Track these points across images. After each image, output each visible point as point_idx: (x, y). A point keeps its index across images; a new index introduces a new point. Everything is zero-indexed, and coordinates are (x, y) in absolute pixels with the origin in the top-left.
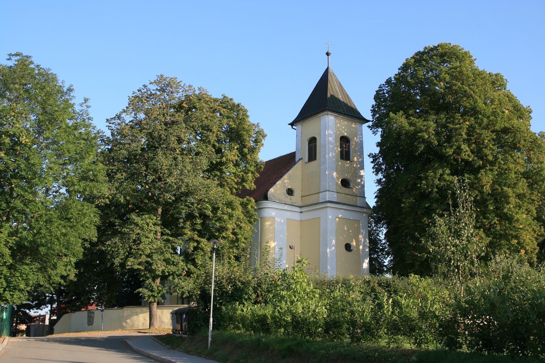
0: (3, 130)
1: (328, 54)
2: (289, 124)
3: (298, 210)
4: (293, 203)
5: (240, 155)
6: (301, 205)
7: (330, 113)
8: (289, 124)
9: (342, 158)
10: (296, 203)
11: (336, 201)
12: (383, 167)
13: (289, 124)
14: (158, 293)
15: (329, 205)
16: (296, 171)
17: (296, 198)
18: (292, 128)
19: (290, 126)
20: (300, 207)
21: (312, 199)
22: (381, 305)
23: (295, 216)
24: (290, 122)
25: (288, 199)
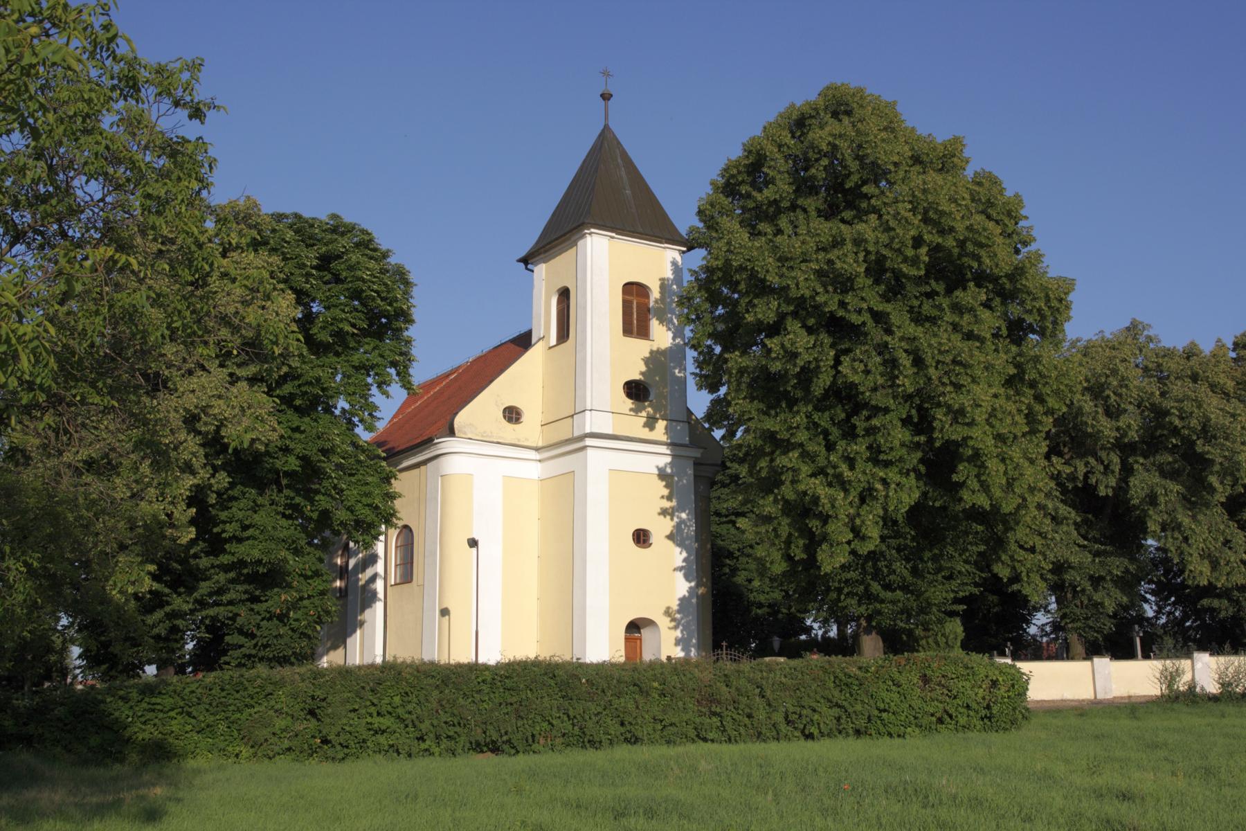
0: (4, 301)
1: (606, 97)
3: (533, 455)
4: (519, 440)
5: (1064, 510)
6: (540, 444)
7: (593, 230)
8: (520, 261)
10: (527, 439)
11: (610, 432)
12: (718, 434)
14: (144, 730)
15: (589, 442)
16: (532, 364)
17: (531, 429)
18: (527, 269)
19: (522, 265)
20: (537, 449)
21: (563, 432)
22: (727, 184)
23: (531, 469)
24: (523, 254)
25: (510, 431)
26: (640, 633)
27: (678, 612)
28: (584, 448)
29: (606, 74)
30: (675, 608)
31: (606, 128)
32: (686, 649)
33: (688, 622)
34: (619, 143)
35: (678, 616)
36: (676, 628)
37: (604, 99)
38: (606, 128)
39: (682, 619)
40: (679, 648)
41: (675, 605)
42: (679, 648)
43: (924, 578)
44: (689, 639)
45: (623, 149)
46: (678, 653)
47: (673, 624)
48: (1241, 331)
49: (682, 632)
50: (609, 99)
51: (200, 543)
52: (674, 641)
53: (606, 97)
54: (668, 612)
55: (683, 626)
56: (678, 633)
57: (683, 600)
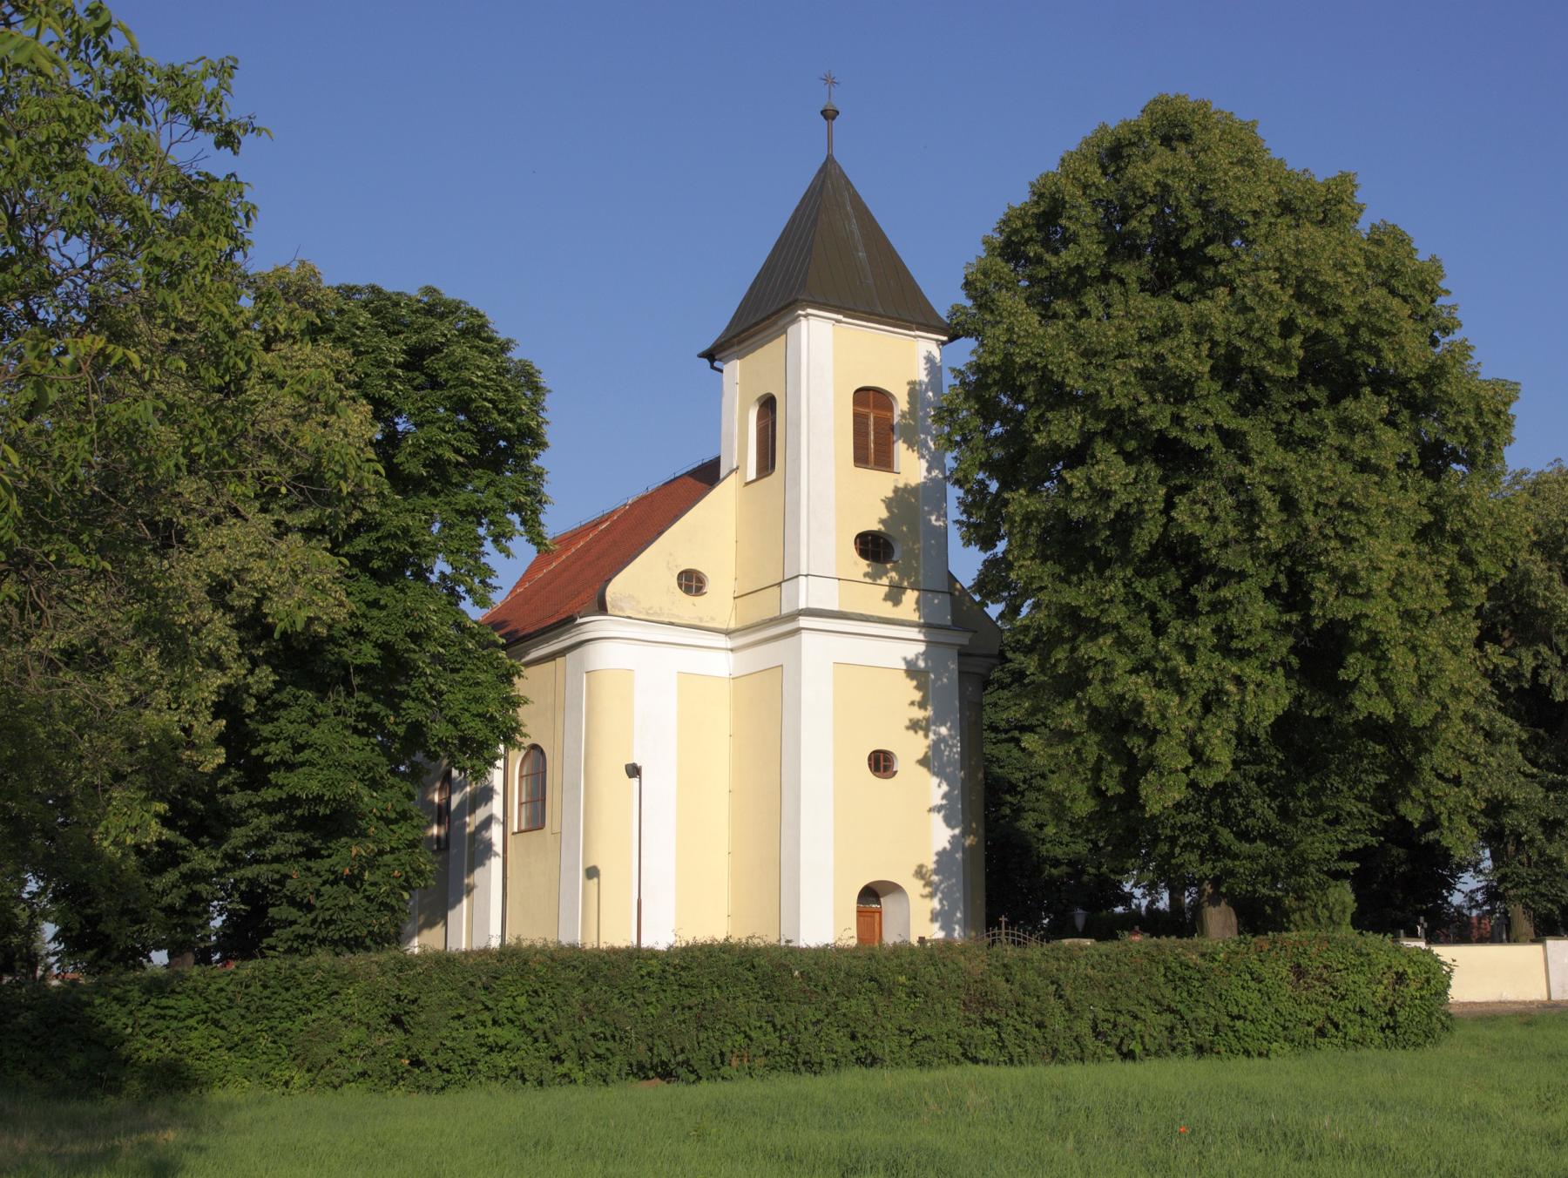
1: (829, 115)
2: (702, 356)
7: (810, 311)
9: (861, 459)
11: (835, 607)
13: (702, 356)
18: (713, 367)
19: (706, 362)
26: (879, 903)
27: (936, 872)
28: (798, 630)
29: (830, 81)
30: (931, 866)
31: (830, 160)
34: (848, 182)
35: (935, 878)
37: (826, 118)
38: (830, 160)
39: (941, 882)
40: (937, 925)
41: (930, 863)
42: (937, 925)
43: (1298, 822)
47: (928, 890)
49: (941, 901)
50: (833, 119)
53: (829, 115)
54: (920, 873)
55: (942, 892)
56: (935, 904)
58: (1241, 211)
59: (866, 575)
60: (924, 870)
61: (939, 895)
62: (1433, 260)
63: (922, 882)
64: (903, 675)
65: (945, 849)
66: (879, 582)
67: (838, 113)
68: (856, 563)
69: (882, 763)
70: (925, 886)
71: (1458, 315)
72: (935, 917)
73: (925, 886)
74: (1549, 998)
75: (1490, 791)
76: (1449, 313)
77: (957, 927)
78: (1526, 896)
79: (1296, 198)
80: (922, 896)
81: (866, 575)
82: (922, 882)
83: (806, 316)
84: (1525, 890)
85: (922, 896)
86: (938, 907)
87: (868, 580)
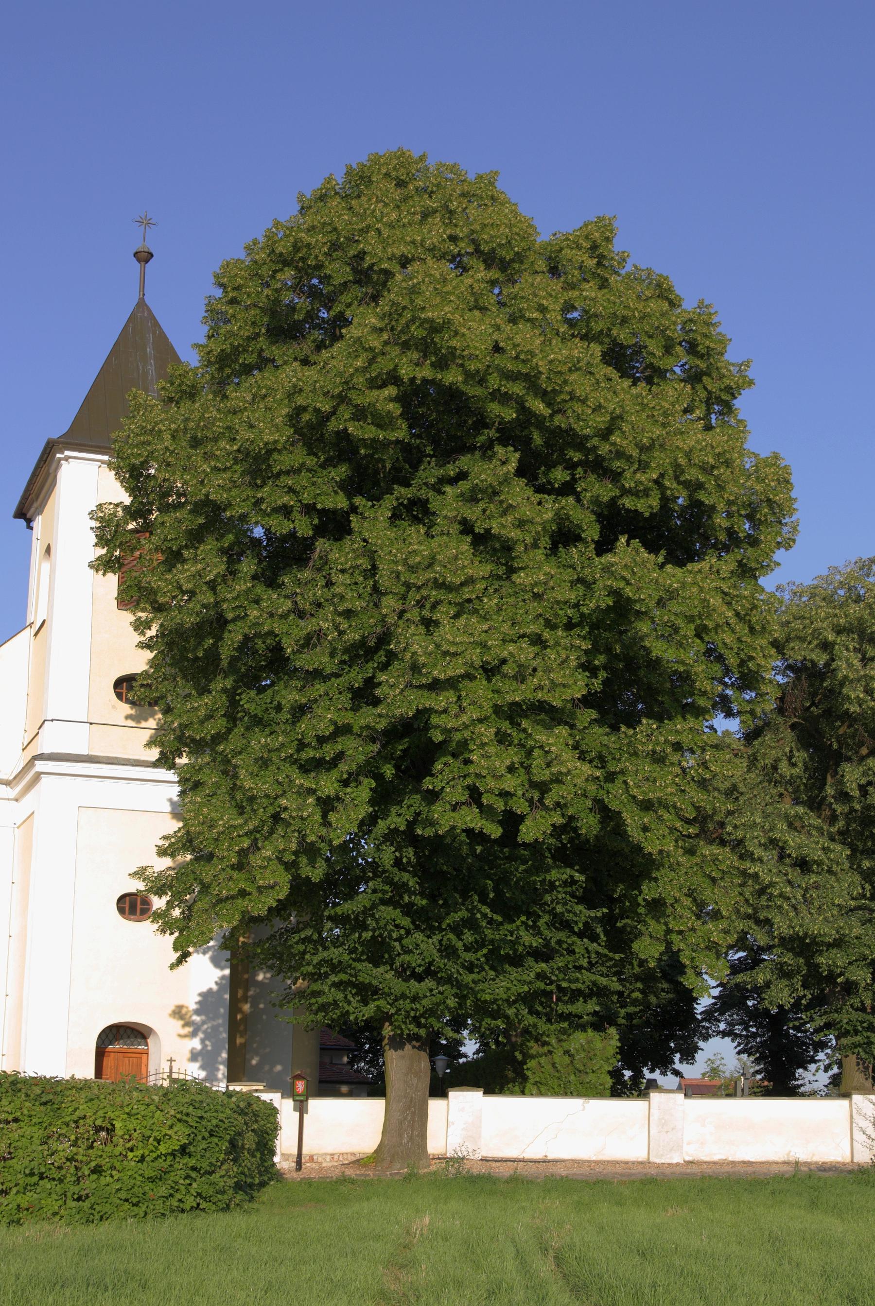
1: (144, 257)
7: (68, 453)
11: (85, 752)
26: (147, 1045)
27: (197, 1012)
28: (38, 776)
29: (146, 223)
30: (193, 1006)
31: (142, 304)
32: (209, 1065)
33: (215, 1029)
34: (156, 324)
35: (196, 1018)
36: (193, 1034)
37: (139, 261)
38: (142, 304)
39: (204, 1023)
40: (196, 1065)
41: (191, 1002)
42: (196, 1065)
43: (459, 957)
44: (216, 1052)
45: (162, 333)
46: (194, 1071)
47: (188, 1030)
48: (871, 555)
49: (202, 1041)
50: (147, 261)
51: (762, 918)
52: (188, 1055)
53: (144, 257)
54: (178, 1013)
55: (205, 1032)
56: (196, 1043)
57: (207, 998)
58: (381, 259)
59: (128, 717)
60: (184, 1011)
61: (201, 1035)
62: (701, 305)
63: (181, 1022)
64: (169, 816)
65: (210, 991)
66: (144, 724)
67: (152, 256)
68: (114, 707)
69: (139, 906)
70: (184, 1026)
71: (750, 374)
72: (194, 1056)
73: (184, 1026)
74: (852, 1161)
75: (790, 927)
76: (740, 371)
77: (221, 1067)
78: (860, 1045)
79: (500, 245)
80: (180, 1036)
81: (128, 717)
82: (181, 1022)
83: (67, 459)
84: (858, 1039)
85: (180, 1036)
86: (199, 1047)
87: (133, 724)
